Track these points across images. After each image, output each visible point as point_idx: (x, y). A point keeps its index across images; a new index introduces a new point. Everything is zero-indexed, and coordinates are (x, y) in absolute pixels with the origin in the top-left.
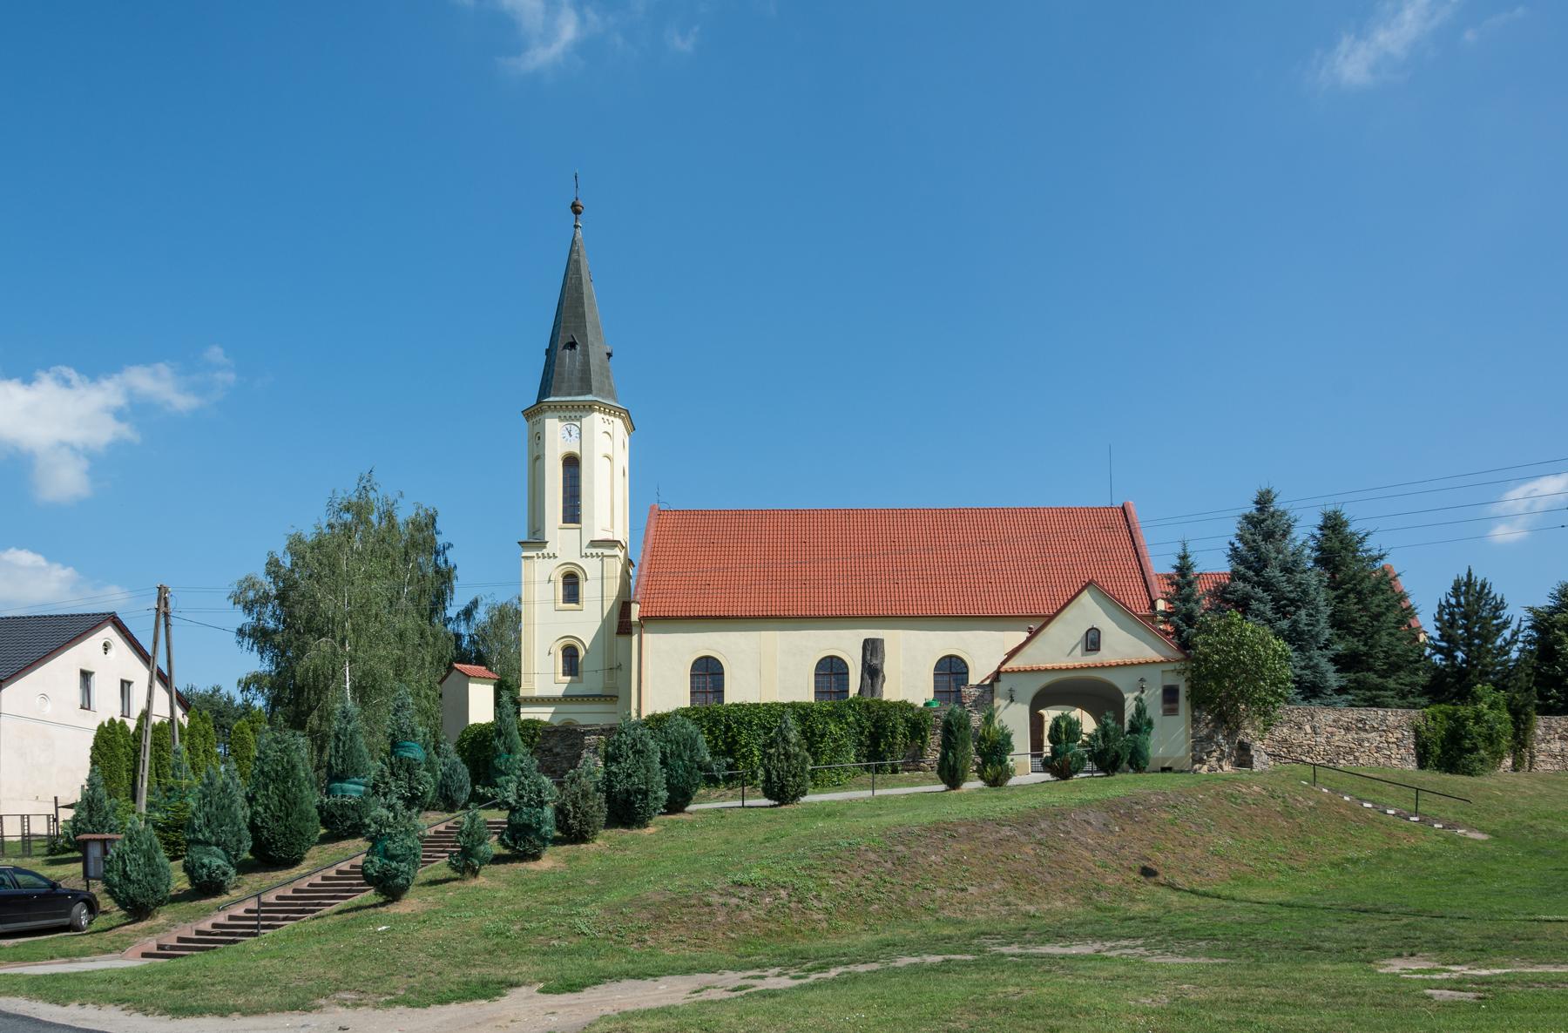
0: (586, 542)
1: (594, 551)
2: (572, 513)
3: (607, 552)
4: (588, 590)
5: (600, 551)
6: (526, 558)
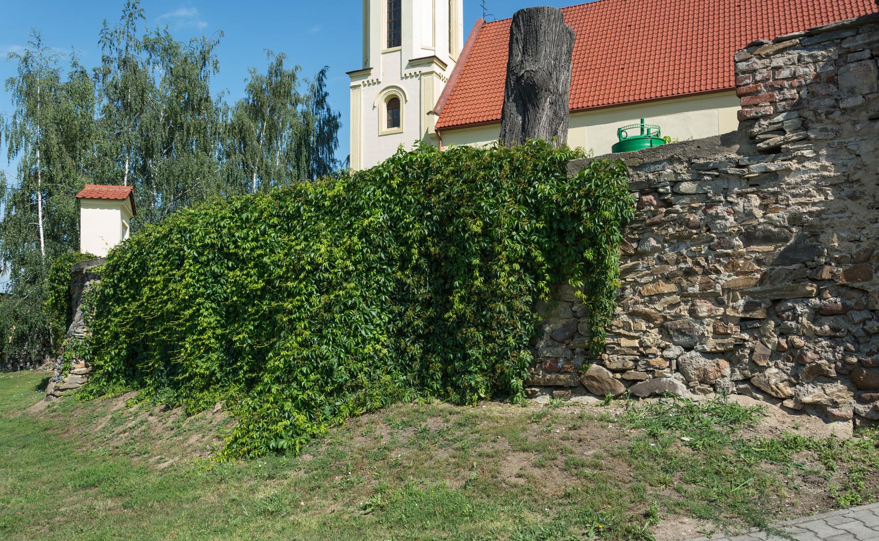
0: (405, 63)
1: (412, 71)
2: (395, 39)
3: (424, 69)
4: (407, 112)
5: (417, 70)
6: (354, 87)
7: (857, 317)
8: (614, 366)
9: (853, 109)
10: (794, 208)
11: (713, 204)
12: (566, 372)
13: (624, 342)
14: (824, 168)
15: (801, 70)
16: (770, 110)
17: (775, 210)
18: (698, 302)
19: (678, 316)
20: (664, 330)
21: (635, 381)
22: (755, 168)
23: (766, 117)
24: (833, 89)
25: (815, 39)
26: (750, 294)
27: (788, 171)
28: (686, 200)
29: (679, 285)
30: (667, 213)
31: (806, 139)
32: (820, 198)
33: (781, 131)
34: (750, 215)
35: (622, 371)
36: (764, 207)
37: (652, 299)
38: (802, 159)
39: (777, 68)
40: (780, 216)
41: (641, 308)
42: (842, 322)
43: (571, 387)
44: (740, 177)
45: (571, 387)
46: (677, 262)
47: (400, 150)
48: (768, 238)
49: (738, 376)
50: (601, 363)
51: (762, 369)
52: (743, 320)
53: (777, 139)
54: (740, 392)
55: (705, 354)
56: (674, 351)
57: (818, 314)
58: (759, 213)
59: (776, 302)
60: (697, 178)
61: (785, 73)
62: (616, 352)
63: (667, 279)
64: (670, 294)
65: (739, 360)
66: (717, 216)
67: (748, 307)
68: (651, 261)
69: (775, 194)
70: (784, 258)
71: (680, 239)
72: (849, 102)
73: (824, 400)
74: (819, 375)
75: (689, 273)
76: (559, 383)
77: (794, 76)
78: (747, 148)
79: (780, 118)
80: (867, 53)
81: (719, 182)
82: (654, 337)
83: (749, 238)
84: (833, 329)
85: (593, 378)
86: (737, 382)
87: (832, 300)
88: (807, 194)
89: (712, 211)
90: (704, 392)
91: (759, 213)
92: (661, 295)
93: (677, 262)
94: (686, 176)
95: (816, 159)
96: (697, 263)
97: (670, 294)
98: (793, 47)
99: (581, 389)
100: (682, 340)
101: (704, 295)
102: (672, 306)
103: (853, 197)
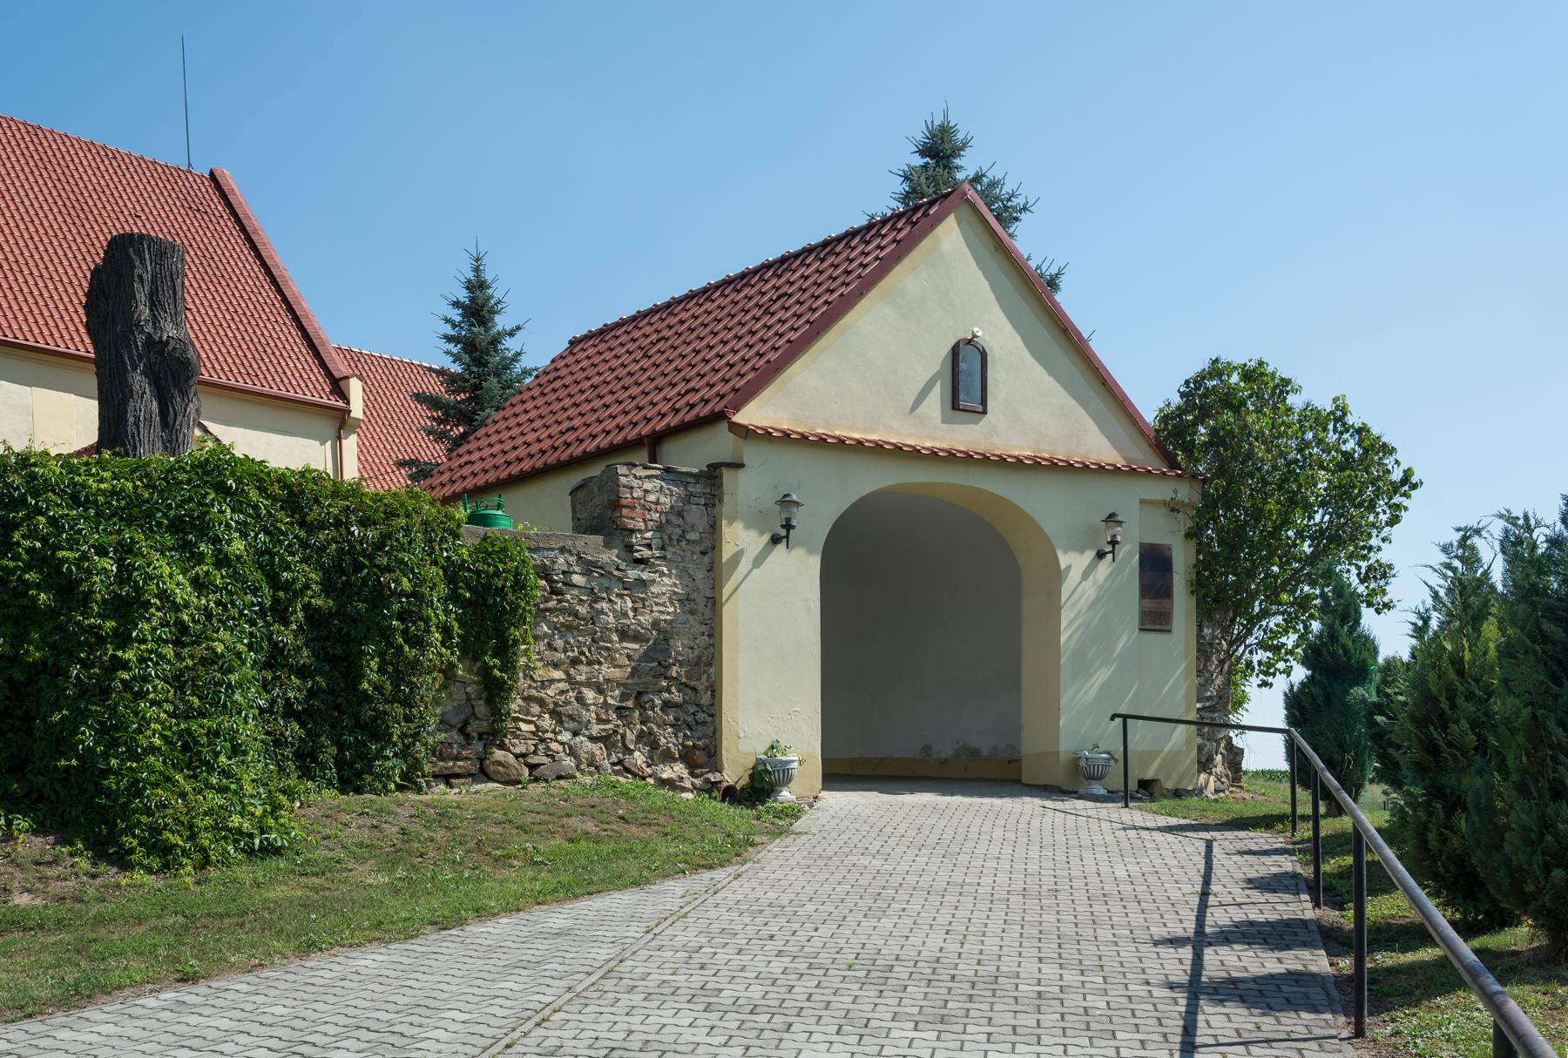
7: (692, 709)
8: (517, 751)
9: (693, 542)
10: (656, 615)
11: (597, 599)
12: (467, 758)
13: (523, 726)
14: (675, 585)
15: (663, 499)
16: (641, 525)
17: (643, 614)
18: (584, 690)
19: (567, 703)
20: (555, 714)
21: (538, 765)
22: (633, 574)
23: (640, 531)
24: (681, 522)
25: (671, 476)
26: (625, 685)
27: (654, 581)
28: (576, 592)
29: (567, 673)
30: (560, 601)
31: (663, 558)
32: (671, 610)
33: (649, 547)
34: (625, 615)
35: (524, 755)
36: (635, 610)
37: (545, 684)
38: (662, 574)
39: (646, 491)
40: (646, 619)
41: (534, 692)
42: (681, 715)
43: (470, 775)
44: (620, 579)
45: (470, 775)
46: (565, 651)
47: (927, 749)
48: (636, 638)
49: (614, 759)
50: (502, 747)
51: (631, 752)
52: (618, 708)
53: (646, 553)
54: (616, 773)
55: (592, 739)
56: (565, 737)
57: (667, 705)
58: (631, 614)
59: (640, 694)
60: (587, 573)
61: (652, 498)
62: (517, 737)
63: (556, 666)
64: (559, 681)
65: (614, 745)
66: (602, 612)
67: (624, 697)
68: (542, 646)
69: (643, 600)
70: (646, 656)
71: (569, 627)
72: (692, 536)
73: (674, 776)
74: (668, 757)
75: (575, 662)
76: (457, 770)
77: (657, 503)
78: (623, 554)
79: (649, 535)
80: (702, 501)
81: (603, 580)
82: (547, 722)
83: (624, 635)
84: (676, 719)
85: (499, 763)
86: (614, 764)
87: (677, 696)
88: (663, 605)
89: (598, 606)
90: (591, 774)
91: (631, 614)
92: (552, 681)
93: (565, 651)
94: (577, 569)
95: (669, 576)
96: (583, 653)
97: (559, 681)
98: (656, 477)
99: (484, 774)
100: (572, 725)
101: (588, 684)
102: (562, 692)
103: (692, 612)
